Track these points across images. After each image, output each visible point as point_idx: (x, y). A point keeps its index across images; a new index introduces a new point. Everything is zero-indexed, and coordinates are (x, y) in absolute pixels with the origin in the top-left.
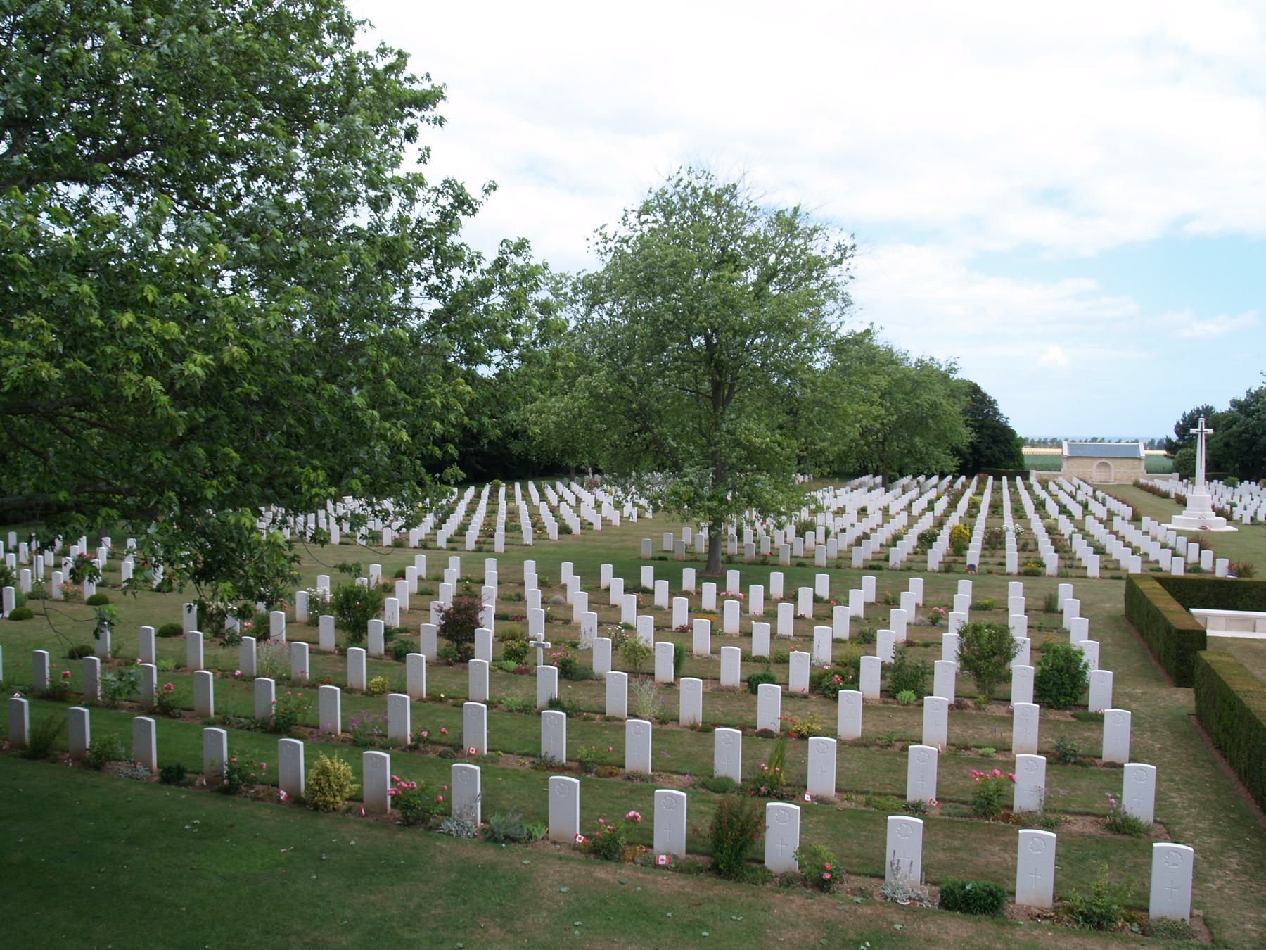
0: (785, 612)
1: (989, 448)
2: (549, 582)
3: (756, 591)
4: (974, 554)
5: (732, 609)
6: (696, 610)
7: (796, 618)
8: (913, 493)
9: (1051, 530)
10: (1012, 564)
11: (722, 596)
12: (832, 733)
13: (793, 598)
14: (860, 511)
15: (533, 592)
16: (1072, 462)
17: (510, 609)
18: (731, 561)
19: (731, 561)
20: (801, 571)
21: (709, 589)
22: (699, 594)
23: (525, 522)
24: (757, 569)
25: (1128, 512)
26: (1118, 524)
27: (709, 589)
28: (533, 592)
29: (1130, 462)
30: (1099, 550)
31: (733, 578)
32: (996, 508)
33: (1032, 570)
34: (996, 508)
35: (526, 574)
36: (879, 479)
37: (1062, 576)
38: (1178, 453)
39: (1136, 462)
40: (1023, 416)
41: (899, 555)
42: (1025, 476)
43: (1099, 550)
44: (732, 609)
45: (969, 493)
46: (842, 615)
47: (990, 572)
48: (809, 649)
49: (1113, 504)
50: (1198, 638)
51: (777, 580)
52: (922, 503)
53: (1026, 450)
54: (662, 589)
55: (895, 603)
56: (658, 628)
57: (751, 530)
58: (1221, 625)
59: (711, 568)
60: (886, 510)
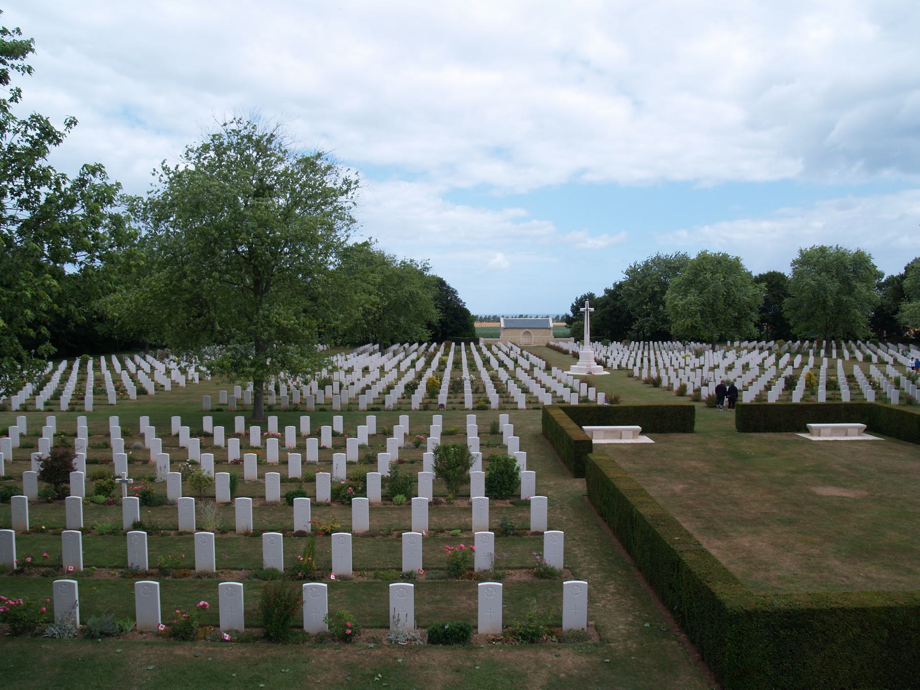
0: (312, 444)
1: (450, 322)
2: (130, 432)
3: (290, 431)
4: (443, 397)
5: (273, 445)
6: (245, 447)
7: (320, 448)
8: (401, 356)
9: (494, 378)
10: (469, 403)
11: (265, 435)
12: (348, 529)
14: (364, 370)
15: (117, 440)
16: (506, 331)
17: (98, 455)
18: (271, 410)
19: (271, 410)
20: (322, 414)
21: (255, 431)
22: (247, 435)
23: (110, 387)
25: (543, 364)
26: (537, 372)
27: (255, 431)
28: (117, 440)
29: (544, 331)
30: (525, 391)
31: (273, 422)
32: (457, 364)
33: (482, 406)
34: (457, 364)
35: (111, 427)
36: (377, 346)
37: (502, 409)
38: (573, 324)
39: (548, 331)
40: (476, 302)
41: (391, 400)
42: (477, 342)
43: (525, 391)
44: (273, 445)
45: (439, 355)
46: (353, 445)
47: (454, 409)
48: (330, 470)
49: (534, 359)
50: (587, 445)
51: (305, 422)
52: (420, 364)
53: (477, 325)
54: (219, 432)
55: (390, 434)
56: (217, 462)
57: (284, 386)
58: (601, 436)
59: (257, 414)
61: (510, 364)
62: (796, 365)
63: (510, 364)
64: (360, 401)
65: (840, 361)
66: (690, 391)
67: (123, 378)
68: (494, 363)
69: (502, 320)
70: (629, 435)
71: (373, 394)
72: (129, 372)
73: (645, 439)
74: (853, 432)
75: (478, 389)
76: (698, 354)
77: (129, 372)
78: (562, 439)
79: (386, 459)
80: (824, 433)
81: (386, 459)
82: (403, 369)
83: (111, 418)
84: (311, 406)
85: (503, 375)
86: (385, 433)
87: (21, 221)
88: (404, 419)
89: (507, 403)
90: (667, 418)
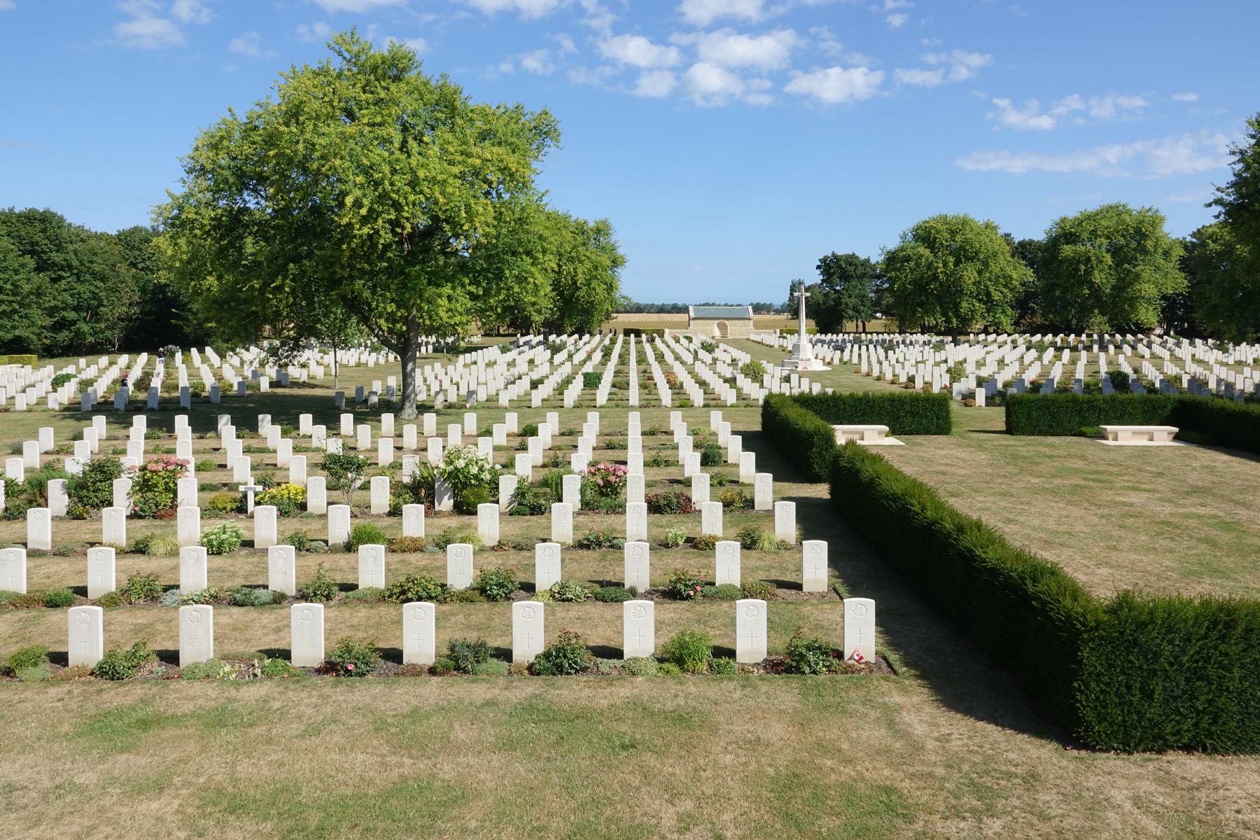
13: (444, 435)
24: (452, 410)
33: (650, 401)
58: (842, 434)
60: (531, 362)
61: (689, 358)
62: (1046, 362)
63: (689, 358)
64: (17, 401)
65: (1102, 355)
66: (919, 384)
67: (202, 370)
68: (669, 357)
69: (691, 308)
70: (874, 437)
71: (546, 390)
72: (211, 366)
73: (893, 441)
74: (1162, 435)
75: (647, 384)
76: (939, 347)
77: (211, 366)
78: (785, 440)
79: (581, 460)
80: (1127, 436)
81: (581, 460)
82: (1026, 361)
83: (301, 416)
84: (439, 404)
85: (681, 374)
86: (570, 433)
87: (1051, 116)
88: (593, 418)
89: (713, 402)
90: (919, 414)
